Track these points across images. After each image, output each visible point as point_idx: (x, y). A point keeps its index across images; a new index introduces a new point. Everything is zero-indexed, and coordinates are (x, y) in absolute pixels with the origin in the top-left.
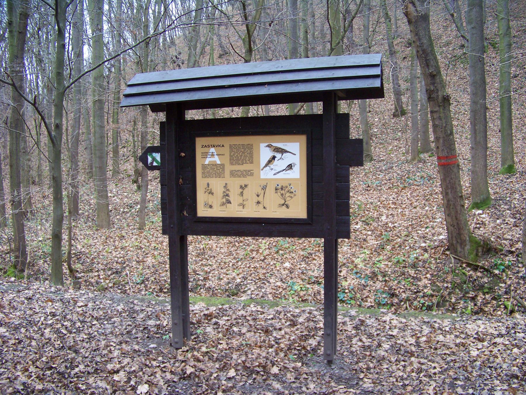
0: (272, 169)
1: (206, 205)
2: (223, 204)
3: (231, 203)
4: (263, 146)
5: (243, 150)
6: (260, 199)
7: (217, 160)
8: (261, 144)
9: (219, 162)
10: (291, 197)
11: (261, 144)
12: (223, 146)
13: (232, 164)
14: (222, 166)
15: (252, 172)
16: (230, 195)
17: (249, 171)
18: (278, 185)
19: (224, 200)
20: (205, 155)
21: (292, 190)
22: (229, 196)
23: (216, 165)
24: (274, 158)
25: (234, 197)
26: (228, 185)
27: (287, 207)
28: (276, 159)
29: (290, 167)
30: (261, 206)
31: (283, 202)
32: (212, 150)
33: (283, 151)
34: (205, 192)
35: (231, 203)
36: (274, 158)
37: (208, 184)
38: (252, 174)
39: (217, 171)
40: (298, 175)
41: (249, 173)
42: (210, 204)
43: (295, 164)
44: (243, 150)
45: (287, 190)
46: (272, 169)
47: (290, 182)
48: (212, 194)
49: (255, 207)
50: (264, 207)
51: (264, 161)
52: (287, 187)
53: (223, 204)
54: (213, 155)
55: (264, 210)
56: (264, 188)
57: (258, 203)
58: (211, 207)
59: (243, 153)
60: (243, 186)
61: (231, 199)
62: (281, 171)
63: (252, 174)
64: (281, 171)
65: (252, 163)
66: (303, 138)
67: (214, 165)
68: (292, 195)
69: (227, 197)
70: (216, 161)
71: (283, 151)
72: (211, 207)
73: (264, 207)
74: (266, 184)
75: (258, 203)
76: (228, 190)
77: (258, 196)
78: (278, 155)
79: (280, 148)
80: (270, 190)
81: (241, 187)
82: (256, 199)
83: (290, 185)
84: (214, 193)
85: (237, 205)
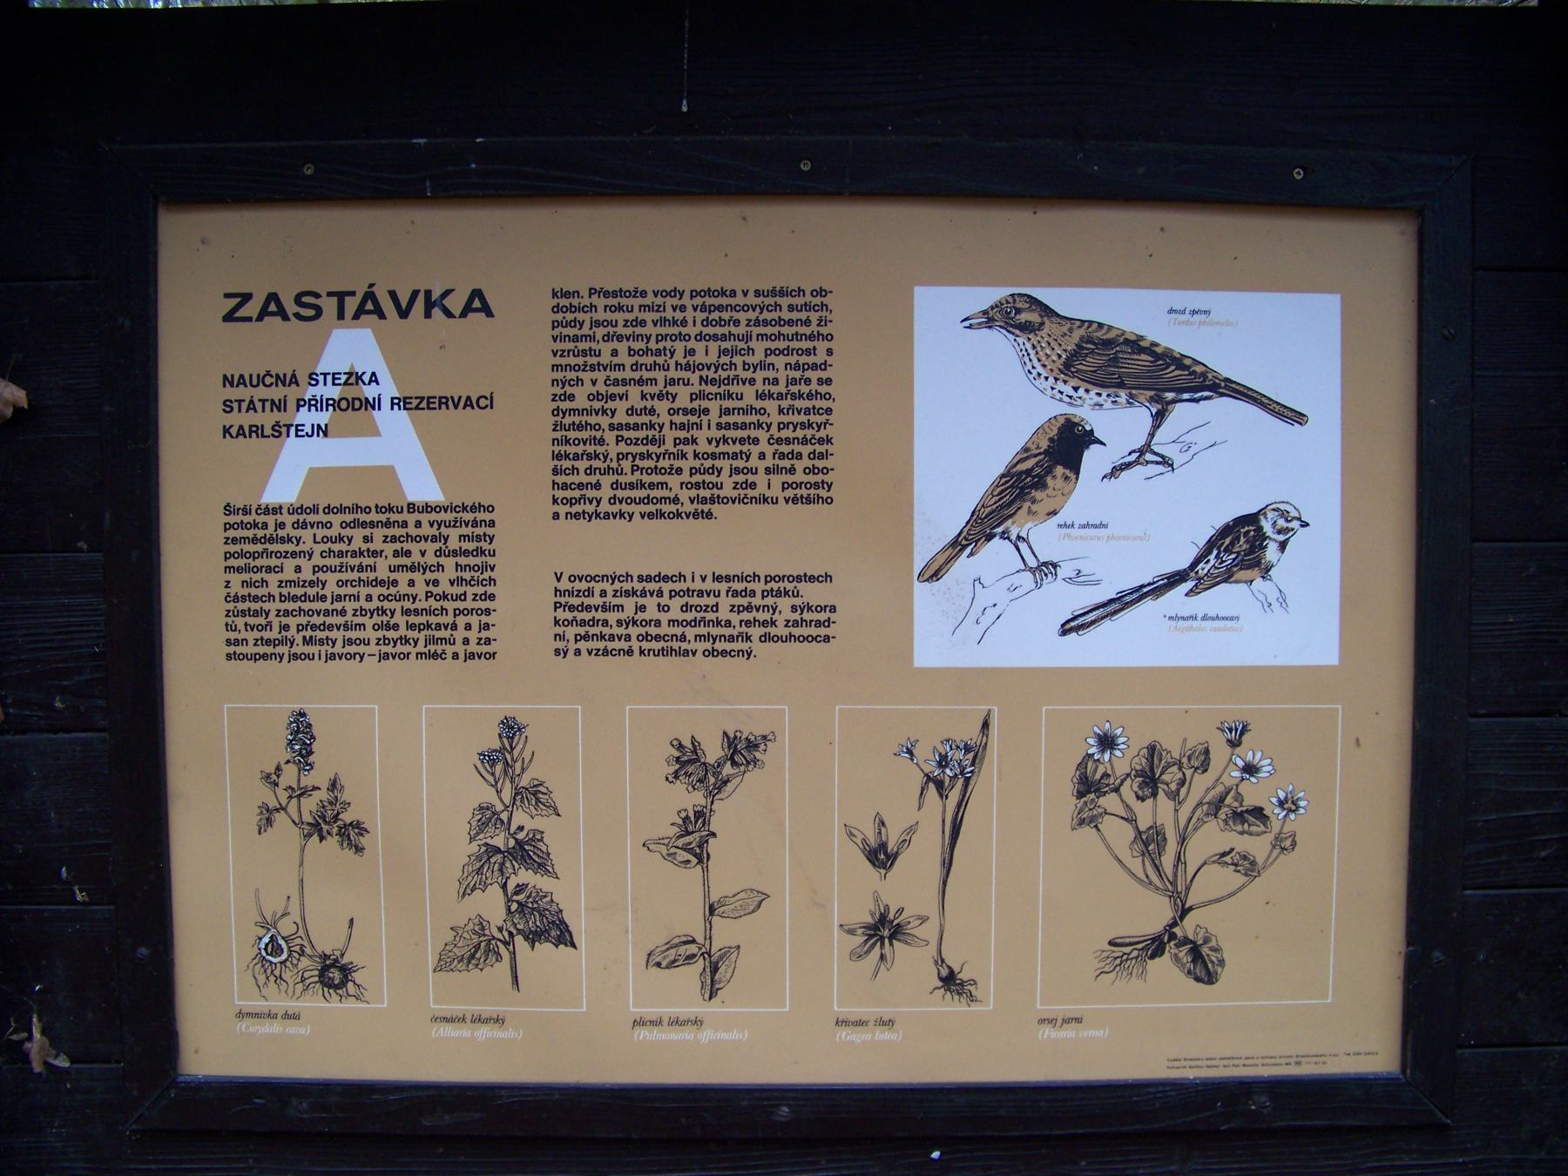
0: (1046, 569)
1: (275, 951)
2: (478, 948)
3: (564, 937)
4: (942, 314)
5: (706, 353)
6: (909, 887)
7: (402, 458)
8: (922, 294)
9: (422, 486)
10: (1249, 867)
11: (922, 294)
12: (478, 303)
13: (574, 502)
14: (468, 528)
15: (812, 593)
16: (554, 843)
17: (780, 585)
18: (1107, 742)
19: (491, 905)
20: (264, 407)
21: (1253, 793)
22: (542, 865)
23: (394, 516)
24: (1068, 445)
25: (605, 867)
26: (535, 739)
27: (1203, 965)
28: (1094, 461)
29: (1241, 546)
30: (912, 964)
31: (1153, 914)
32: (351, 347)
33: (1167, 379)
34: (268, 817)
35: (564, 937)
36: (1068, 445)
37: (301, 734)
38: (815, 625)
39: (399, 583)
40: (1319, 628)
41: (771, 613)
42: (327, 941)
43: (1292, 522)
44: (706, 353)
45: (1200, 785)
46: (1046, 569)
47: (1242, 708)
48: (352, 835)
49: (842, 976)
50: (950, 980)
51: (952, 468)
52: (1203, 760)
53: (478, 948)
54: (354, 404)
55: (953, 1007)
56: (953, 773)
57: (884, 930)
58: (335, 974)
59: (719, 382)
60: (713, 751)
61: (571, 891)
62: (1140, 594)
63: (815, 625)
64: (1140, 594)
65: (814, 493)
66: (1383, 251)
67: (379, 515)
68: (1257, 846)
69: (525, 876)
70: (387, 474)
71: (1167, 379)
72: (335, 974)
73: (950, 980)
74: (971, 733)
75: (884, 930)
76: (534, 795)
77: (881, 856)
78: (1117, 423)
79: (1136, 345)
80: (1023, 797)
81: (687, 761)
82: (855, 891)
83: (1237, 736)
84: (377, 825)
85: (633, 958)
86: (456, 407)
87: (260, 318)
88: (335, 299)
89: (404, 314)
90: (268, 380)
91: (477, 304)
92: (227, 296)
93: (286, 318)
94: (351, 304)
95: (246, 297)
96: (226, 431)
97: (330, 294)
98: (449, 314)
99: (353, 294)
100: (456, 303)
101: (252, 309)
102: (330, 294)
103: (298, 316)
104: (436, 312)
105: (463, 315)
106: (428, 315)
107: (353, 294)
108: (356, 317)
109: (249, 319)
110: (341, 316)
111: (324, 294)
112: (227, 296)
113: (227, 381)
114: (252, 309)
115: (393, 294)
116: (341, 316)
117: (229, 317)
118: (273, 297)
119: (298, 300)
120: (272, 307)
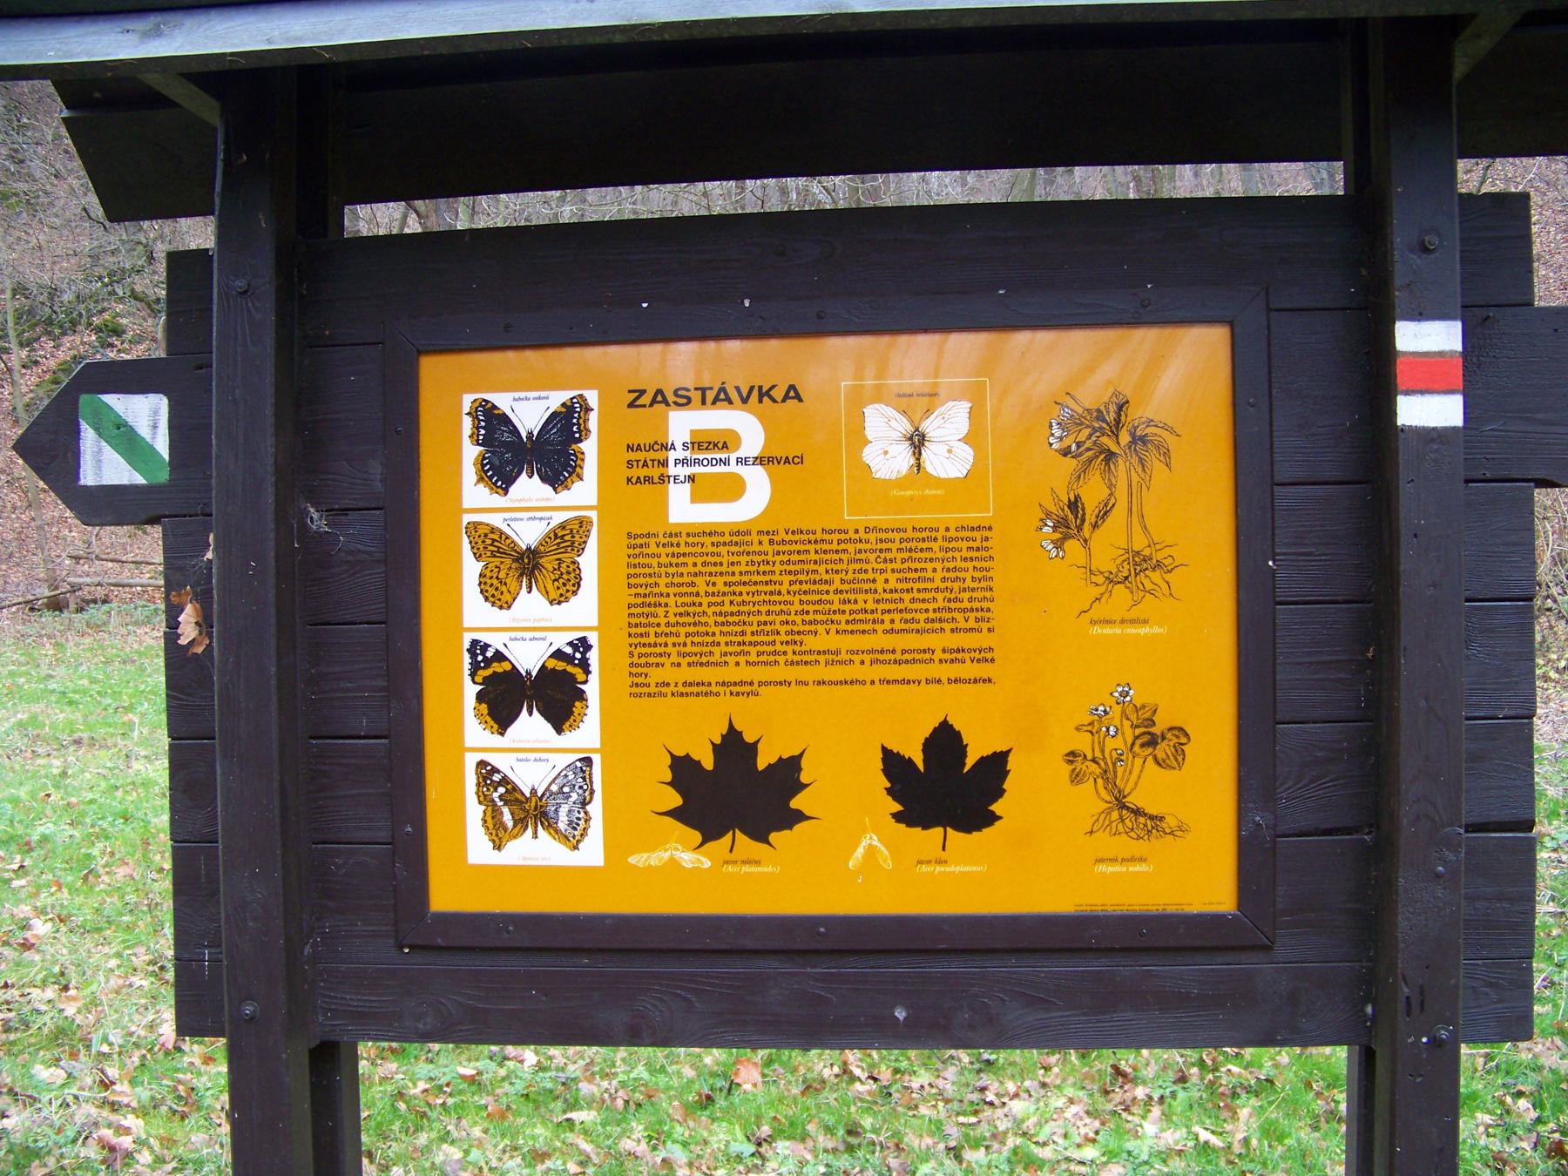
89: (745, 401)
91: (792, 394)
93: (668, 404)
94: (710, 396)
95: (642, 392)
96: (629, 480)
98: (775, 401)
100: (778, 394)
101: (646, 400)
104: (765, 399)
105: (784, 401)
106: (761, 401)
108: (714, 403)
110: (704, 402)
113: (630, 448)
114: (646, 400)
115: (737, 388)
116: (704, 402)
117: (631, 405)
118: (659, 392)
119: (676, 393)
120: (659, 398)
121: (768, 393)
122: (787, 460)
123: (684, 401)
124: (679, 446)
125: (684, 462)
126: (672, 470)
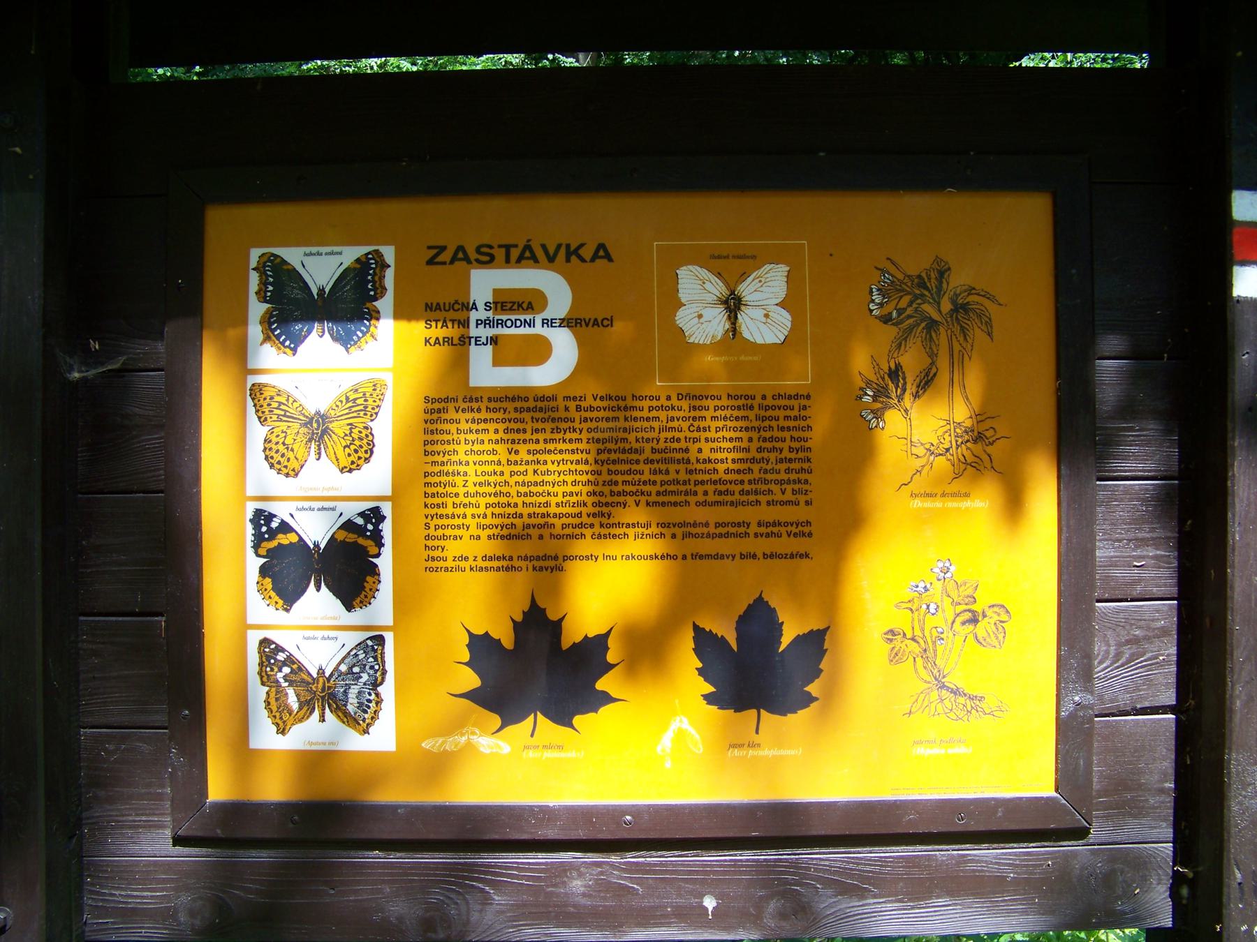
86: (587, 325)
87: (452, 262)
88: (503, 250)
90: (456, 307)
92: (429, 248)
93: (469, 262)
94: (515, 253)
95: (443, 249)
97: (500, 246)
99: (516, 246)
100: (587, 253)
102: (500, 246)
103: (477, 261)
104: (573, 258)
106: (568, 260)
107: (516, 246)
109: (444, 263)
111: (495, 244)
112: (429, 248)
115: (544, 247)
117: (431, 262)
118: (461, 248)
119: (478, 250)
121: (576, 252)
122: (596, 323)
123: (486, 258)
124: (481, 306)
125: (486, 323)
126: (474, 331)
